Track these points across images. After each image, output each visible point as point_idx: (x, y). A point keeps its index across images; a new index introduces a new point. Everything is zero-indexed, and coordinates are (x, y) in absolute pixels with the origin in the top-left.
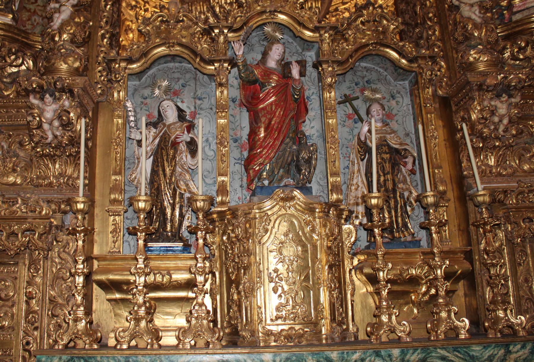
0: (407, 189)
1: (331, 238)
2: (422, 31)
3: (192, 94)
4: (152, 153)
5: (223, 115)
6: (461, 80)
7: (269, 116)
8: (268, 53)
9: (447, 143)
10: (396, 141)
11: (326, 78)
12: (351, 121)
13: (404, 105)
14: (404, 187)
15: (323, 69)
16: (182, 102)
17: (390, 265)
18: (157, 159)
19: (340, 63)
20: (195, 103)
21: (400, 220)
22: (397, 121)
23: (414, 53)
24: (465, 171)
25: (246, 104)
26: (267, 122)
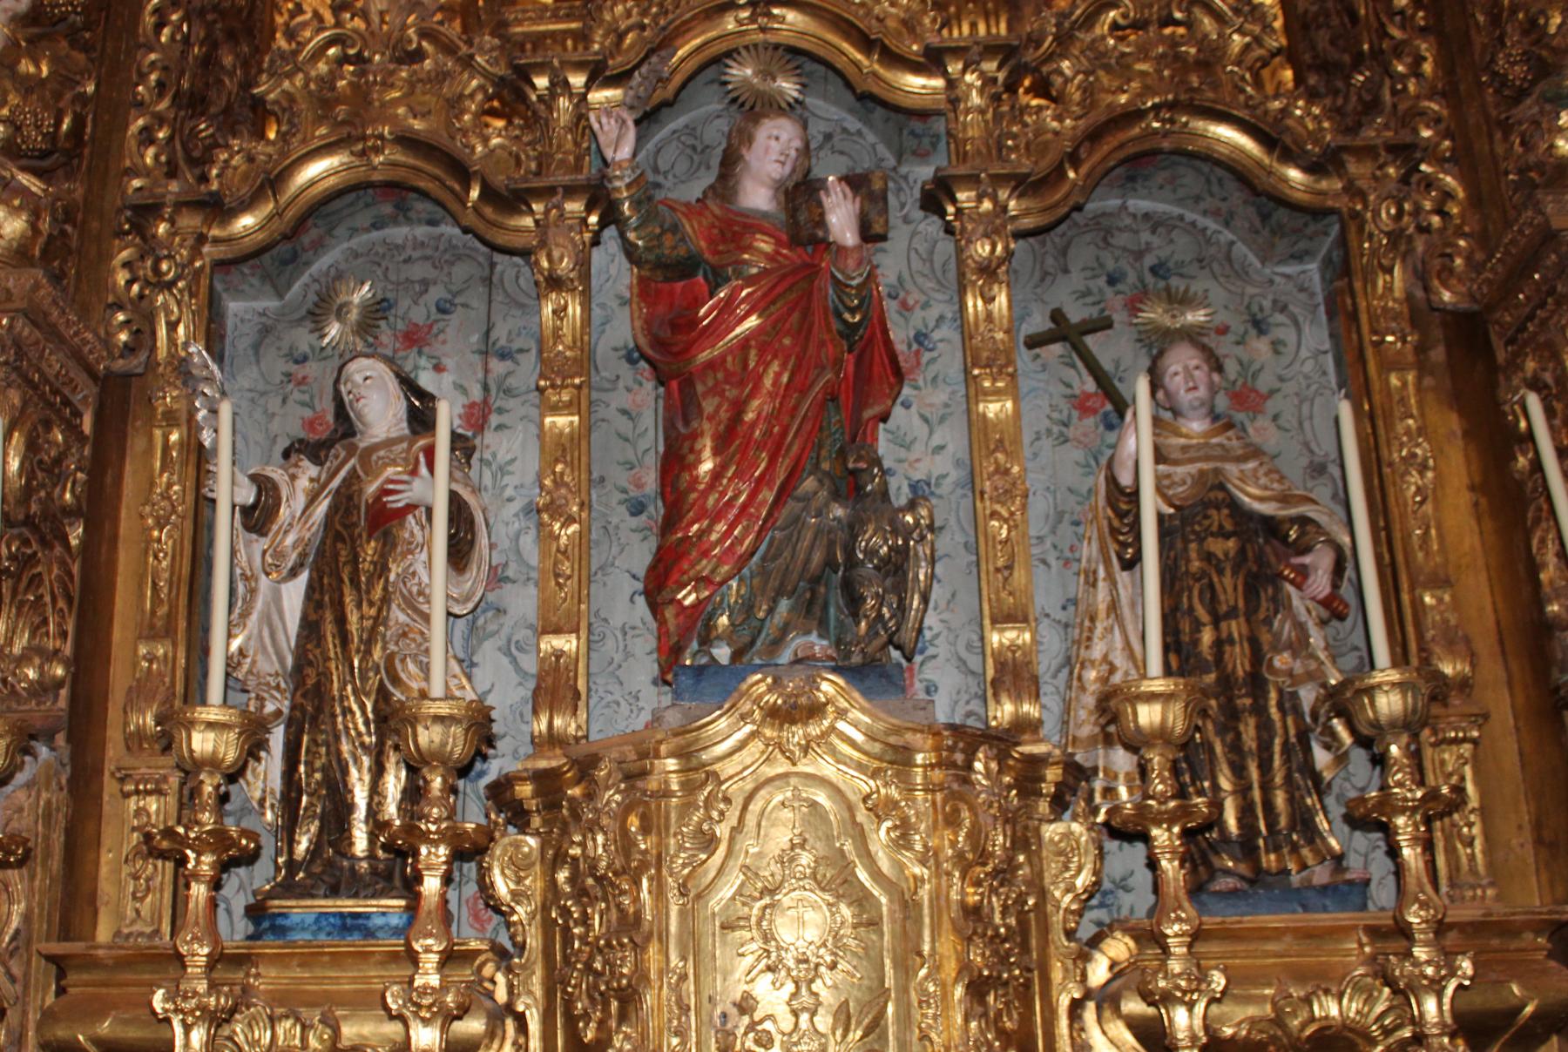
0: (1310, 676)
1: (980, 872)
2: (1377, 78)
3: (475, 338)
4: (303, 555)
5: (565, 397)
6: (1521, 231)
7: (731, 393)
8: (740, 158)
9: (1483, 502)
10: (1266, 488)
11: (969, 242)
12: (1090, 421)
13: (1304, 353)
14: (1298, 667)
15: (959, 212)
16: (438, 368)
17: (1218, 981)
18: (321, 578)
19: (1023, 185)
20: (487, 371)
21: (1280, 799)
22: (1275, 418)
23: (1328, 138)
24: (1550, 602)
25: (650, 352)
26: (724, 415)
